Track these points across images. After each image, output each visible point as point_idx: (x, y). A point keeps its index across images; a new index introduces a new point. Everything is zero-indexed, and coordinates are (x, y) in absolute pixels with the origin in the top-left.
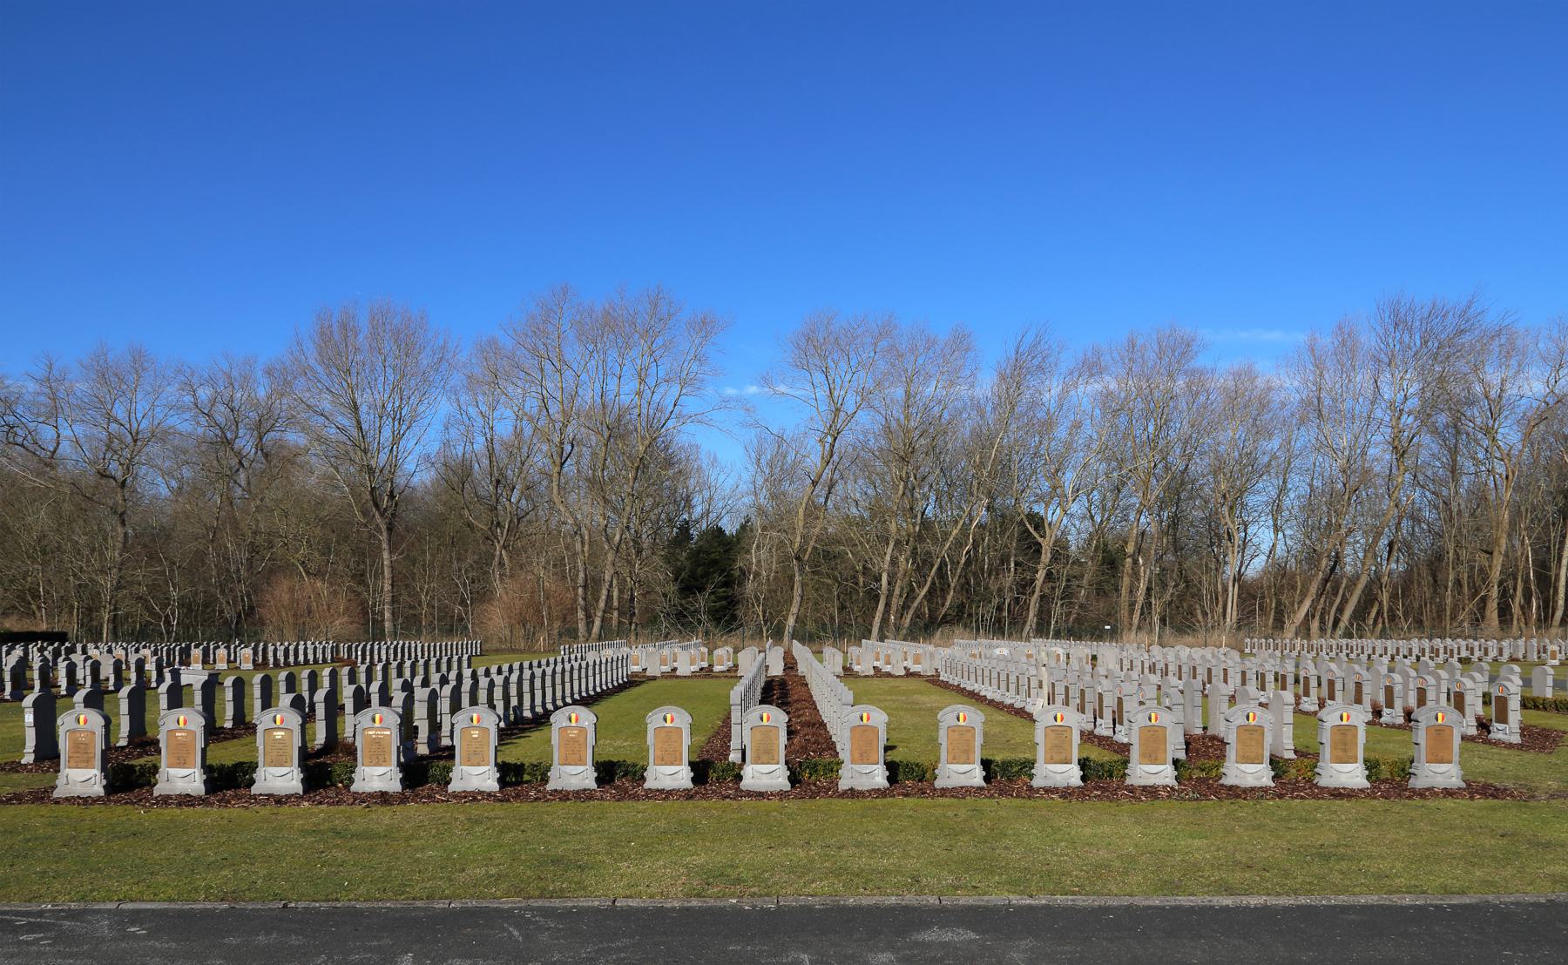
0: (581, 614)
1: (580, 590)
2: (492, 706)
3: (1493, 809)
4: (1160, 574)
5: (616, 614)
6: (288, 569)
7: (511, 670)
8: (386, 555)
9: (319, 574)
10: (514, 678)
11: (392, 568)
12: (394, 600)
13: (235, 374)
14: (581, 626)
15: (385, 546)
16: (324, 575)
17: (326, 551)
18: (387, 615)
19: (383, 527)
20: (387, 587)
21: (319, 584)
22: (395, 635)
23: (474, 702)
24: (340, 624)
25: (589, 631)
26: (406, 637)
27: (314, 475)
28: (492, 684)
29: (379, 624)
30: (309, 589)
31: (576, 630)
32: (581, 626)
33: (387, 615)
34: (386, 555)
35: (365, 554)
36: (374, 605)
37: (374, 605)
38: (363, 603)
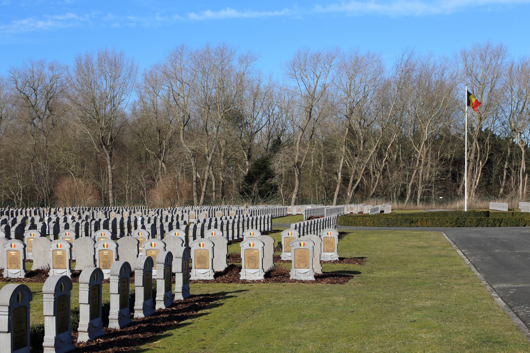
0: (195, 194)
1: (194, 183)
2: (143, 227)
3: (381, 229)
4: (481, 208)
5: (214, 194)
6: (67, 174)
7: (235, 217)
8: (109, 167)
9: (80, 176)
10: (236, 220)
11: (112, 174)
12: (114, 188)
13: (35, 70)
14: (195, 199)
15: (109, 163)
16: (82, 177)
17: (83, 166)
18: (110, 195)
19: (108, 154)
20: (110, 182)
21: (80, 182)
22: (114, 204)
23: (216, 227)
24: (90, 199)
25: (199, 201)
26: (119, 205)
27: (77, 129)
28: (228, 222)
29: (106, 199)
30: (76, 184)
31: (193, 201)
32: (195, 199)
33: (110, 195)
34: (109, 167)
35: (100, 166)
36: (104, 191)
37: (104, 191)
38: (100, 190)
